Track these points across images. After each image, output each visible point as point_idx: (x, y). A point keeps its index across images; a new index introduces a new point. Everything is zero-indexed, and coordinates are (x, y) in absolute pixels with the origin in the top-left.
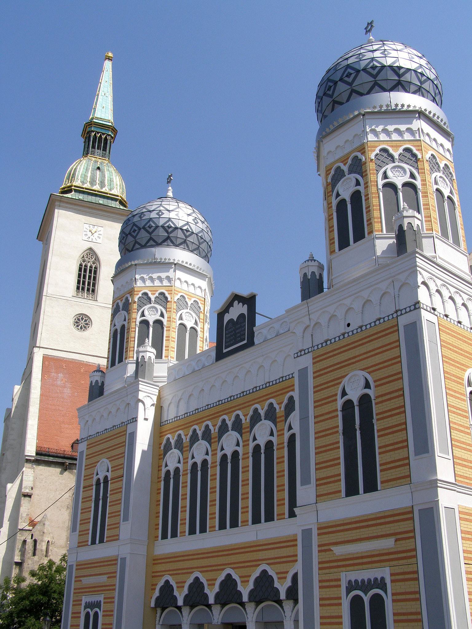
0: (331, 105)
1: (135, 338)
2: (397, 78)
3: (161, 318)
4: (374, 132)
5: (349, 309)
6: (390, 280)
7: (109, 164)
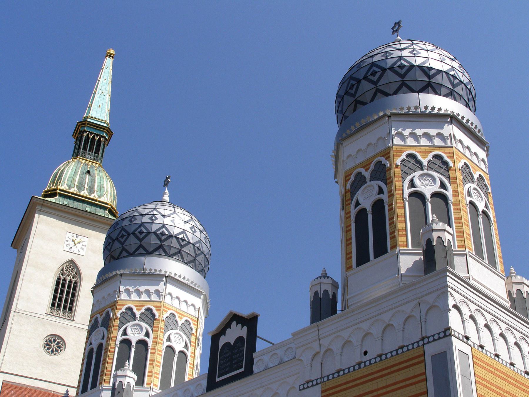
0: (354, 104)
1: (113, 359)
2: (427, 79)
3: (146, 338)
4: (400, 135)
5: (367, 334)
6: (416, 302)
7: (101, 169)
